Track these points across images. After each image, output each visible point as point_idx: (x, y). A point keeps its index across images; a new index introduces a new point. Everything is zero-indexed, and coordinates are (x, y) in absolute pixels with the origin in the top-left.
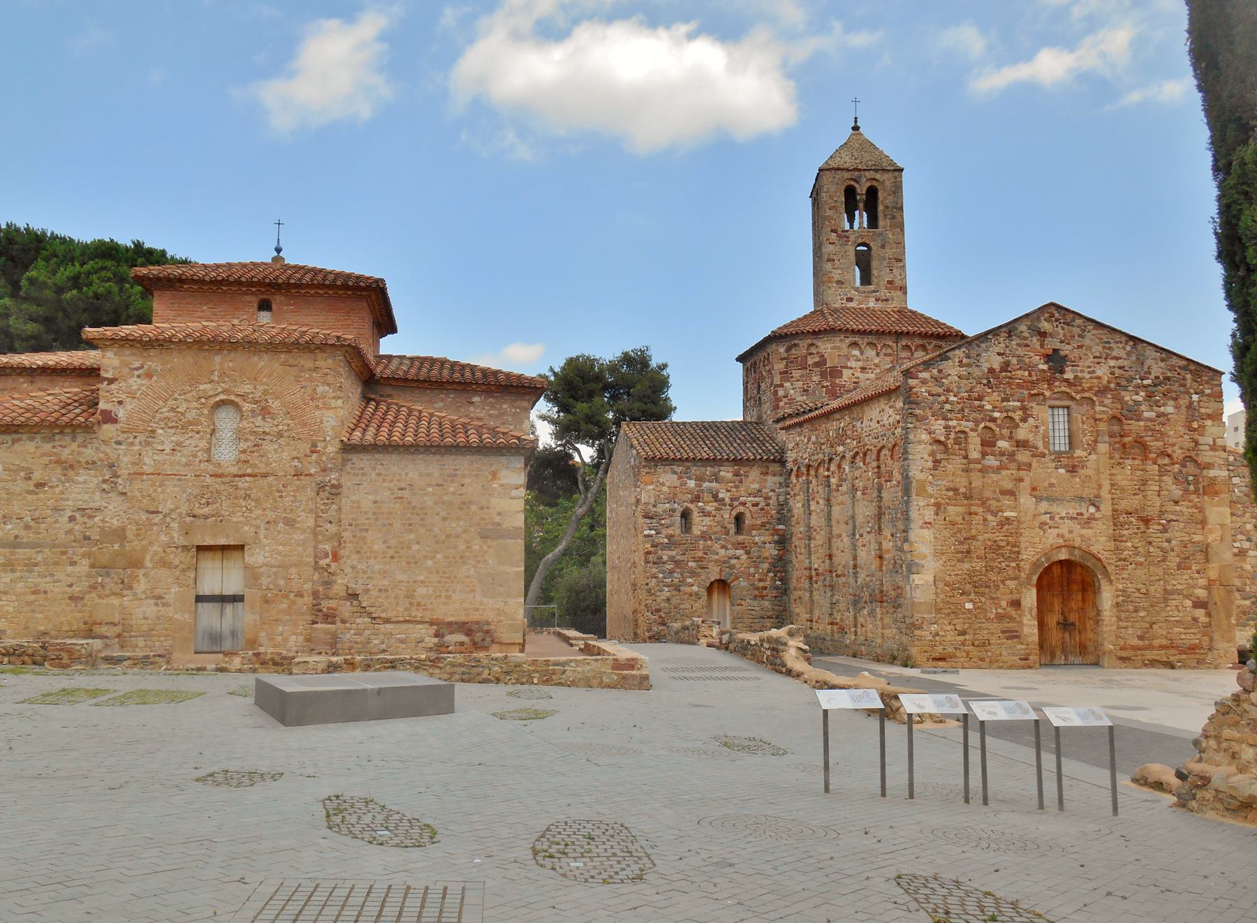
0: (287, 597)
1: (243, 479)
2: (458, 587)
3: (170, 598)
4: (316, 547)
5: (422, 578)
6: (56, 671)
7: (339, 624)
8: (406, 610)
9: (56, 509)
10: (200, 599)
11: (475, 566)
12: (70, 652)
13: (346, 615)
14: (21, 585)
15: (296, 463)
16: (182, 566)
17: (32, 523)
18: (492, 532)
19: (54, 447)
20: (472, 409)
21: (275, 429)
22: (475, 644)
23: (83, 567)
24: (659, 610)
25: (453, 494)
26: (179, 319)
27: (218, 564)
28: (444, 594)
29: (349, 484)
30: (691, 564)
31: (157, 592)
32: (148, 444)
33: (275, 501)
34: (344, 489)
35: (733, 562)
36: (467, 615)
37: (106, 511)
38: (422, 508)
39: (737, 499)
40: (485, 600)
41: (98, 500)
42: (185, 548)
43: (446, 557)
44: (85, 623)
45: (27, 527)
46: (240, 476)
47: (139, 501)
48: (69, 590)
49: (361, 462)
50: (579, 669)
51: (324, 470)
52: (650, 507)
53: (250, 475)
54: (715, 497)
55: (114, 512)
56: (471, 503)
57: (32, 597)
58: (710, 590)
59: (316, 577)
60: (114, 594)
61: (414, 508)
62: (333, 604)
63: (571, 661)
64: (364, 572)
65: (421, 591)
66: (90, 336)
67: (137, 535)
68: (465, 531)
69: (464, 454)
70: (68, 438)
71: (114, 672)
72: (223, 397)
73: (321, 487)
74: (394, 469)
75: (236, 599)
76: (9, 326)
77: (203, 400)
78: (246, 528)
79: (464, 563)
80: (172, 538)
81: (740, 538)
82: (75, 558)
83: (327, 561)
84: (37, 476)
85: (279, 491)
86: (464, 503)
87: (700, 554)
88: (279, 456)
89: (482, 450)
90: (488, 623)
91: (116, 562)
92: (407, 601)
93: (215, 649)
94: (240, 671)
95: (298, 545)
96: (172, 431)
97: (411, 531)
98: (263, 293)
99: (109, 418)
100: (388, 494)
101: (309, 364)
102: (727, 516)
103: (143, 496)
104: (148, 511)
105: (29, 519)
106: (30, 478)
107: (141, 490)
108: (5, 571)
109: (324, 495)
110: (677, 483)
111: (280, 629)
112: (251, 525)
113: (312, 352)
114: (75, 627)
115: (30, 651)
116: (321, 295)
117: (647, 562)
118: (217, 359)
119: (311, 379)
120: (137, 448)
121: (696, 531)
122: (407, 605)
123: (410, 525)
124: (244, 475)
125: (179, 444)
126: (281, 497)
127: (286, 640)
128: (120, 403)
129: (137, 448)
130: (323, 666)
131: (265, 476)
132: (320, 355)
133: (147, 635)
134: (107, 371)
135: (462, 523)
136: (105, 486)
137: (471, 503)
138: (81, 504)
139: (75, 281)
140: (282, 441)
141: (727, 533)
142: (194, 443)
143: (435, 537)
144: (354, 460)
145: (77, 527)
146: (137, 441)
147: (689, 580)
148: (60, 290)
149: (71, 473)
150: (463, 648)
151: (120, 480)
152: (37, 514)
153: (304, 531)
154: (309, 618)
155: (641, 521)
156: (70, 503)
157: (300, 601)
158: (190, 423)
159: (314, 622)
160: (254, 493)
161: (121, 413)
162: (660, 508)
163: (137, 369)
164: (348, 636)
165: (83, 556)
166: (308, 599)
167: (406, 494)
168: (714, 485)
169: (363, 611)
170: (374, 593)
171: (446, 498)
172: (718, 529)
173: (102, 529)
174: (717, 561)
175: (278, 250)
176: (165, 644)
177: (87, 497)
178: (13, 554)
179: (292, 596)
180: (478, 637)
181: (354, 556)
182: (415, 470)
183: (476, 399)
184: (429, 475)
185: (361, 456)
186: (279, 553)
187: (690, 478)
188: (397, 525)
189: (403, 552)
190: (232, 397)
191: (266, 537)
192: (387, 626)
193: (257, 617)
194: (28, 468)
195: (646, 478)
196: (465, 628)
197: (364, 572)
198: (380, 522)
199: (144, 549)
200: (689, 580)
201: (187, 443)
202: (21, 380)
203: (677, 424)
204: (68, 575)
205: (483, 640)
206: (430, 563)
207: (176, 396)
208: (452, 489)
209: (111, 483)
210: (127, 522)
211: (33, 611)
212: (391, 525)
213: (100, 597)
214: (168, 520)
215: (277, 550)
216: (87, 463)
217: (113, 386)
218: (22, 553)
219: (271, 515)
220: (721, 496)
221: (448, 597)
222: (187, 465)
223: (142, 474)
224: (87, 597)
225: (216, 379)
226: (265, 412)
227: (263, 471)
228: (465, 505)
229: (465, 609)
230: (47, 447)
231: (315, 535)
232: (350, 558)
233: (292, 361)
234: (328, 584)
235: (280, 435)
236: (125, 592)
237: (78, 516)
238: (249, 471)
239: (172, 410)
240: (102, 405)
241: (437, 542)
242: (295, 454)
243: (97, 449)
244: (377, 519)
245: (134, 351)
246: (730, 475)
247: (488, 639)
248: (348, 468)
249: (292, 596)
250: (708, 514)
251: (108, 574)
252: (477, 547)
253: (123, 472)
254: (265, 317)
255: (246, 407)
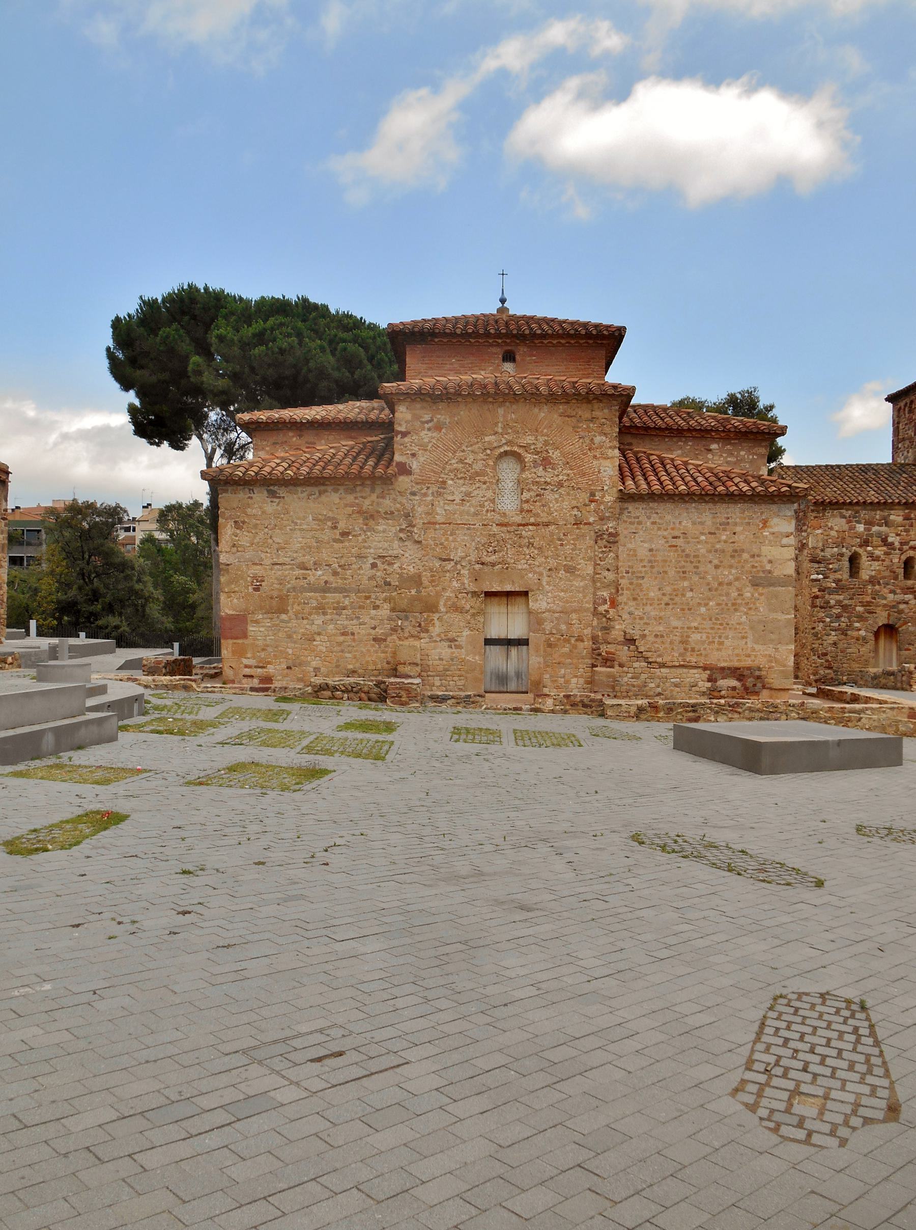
0: (568, 641)
1: (527, 528)
2: (731, 634)
3: (462, 640)
4: (595, 594)
5: (696, 624)
6: (397, 707)
7: (617, 667)
8: (681, 655)
9: (360, 557)
10: (489, 642)
11: (746, 614)
12: (408, 691)
13: (624, 659)
14: (331, 626)
15: (575, 512)
16: (472, 611)
17: (339, 570)
18: (763, 580)
19: (356, 498)
20: (710, 456)
21: (556, 479)
22: (746, 689)
23: (385, 611)
24: (825, 654)
25: (725, 542)
26: (430, 372)
27: (503, 609)
28: (716, 640)
29: (626, 532)
30: (858, 609)
31: (450, 635)
32: (440, 494)
33: (556, 549)
34: (621, 538)
35: (902, 606)
36: (739, 660)
37: (404, 559)
38: (695, 556)
39: (906, 543)
40: (756, 646)
41: (396, 548)
42: (475, 594)
43: (718, 604)
44: (388, 663)
45: (335, 573)
46: (524, 525)
47: (434, 549)
48: (373, 632)
49: (636, 510)
50: (875, 717)
51: (602, 519)
52: (818, 551)
53: (532, 524)
54: (885, 541)
55: (410, 560)
56: (743, 551)
57: (342, 638)
58: (877, 634)
59: (595, 623)
60: (412, 636)
61: (687, 556)
62: (611, 648)
63: (867, 709)
64: (641, 618)
65: (695, 637)
66: (388, 391)
67: (433, 581)
68: (737, 579)
69: (736, 502)
70: (368, 490)
71: (440, 709)
72: (506, 448)
73: (599, 536)
74: (668, 517)
75: (522, 642)
76: (202, 383)
77: (488, 452)
78: (530, 575)
79: (736, 610)
80: (463, 584)
81: (910, 583)
82: (378, 603)
83: (606, 607)
84: (342, 525)
85: (560, 540)
86: (735, 551)
87: (868, 599)
88: (560, 506)
89: (754, 498)
90: (759, 669)
91: (414, 607)
92: (682, 646)
93: (502, 689)
94: (553, 711)
95: (579, 592)
96: (461, 481)
97: (684, 579)
98: (507, 344)
99: (404, 470)
100: (662, 542)
101: (587, 415)
102: (897, 559)
103: (436, 545)
104: (440, 559)
105: (336, 565)
106: (336, 528)
107: (434, 539)
108: (318, 614)
109: (602, 543)
110: (846, 527)
111: (563, 671)
112: (535, 572)
113: (589, 402)
114: (379, 666)
115: (366, 689)
116: (563, 345)
117: (814, 606)
118: (501, 411)
119: (588, 430)
120: (430, 498)
121: (865, 575)
122: (682, 650)
123: (684, 572)
124: (527, 524)
125: (468, 494)
126: (562, 545)
127: (567, 682)
128: (414, 455)
129: (430, 498)
130: (633, 710)
131: (547, 525)
132: (596, 405)
133: (442, 675)
134: (400, 425)
135: (734, 571)
136: (401, 535)
137: (743, 551)
138: (381, 552)
139: (260, 338)
140: (562, 490)
141: (896, 578)
142: (481, 493)
143: (708, 584)
144: (630, 509)
145: (379, 574)
146: (430, 491)
147: (857, 625)
148: (245, 346)
149: (371, 523)
150: (735, 693)
151: (415, 530)
152: (343, 562)
153: (584, 579)
154: (589, 661)
155: (806, 565)
156: (372, 551)
157: (581, 645)
158: (477, 474)
159: (594, 666)
160: (537, 542)
161: (415, 465)
162: (828, 553)
163: (427, 422)
164: (626, 679)
165: (385, 600)
166: (588, 644)
167: (680, 542)
168: (884, 529)
169: (640, 655)
170: (651, 638)
171: (718, 546)
172: (887, 573)
173: (401, 575)
174: (885, 606)
175: (503, 301)
176: (459, 683)
177: (386, 545)
178: (324, 598)
179: (573, 640)
180: (750, 682)
181: (632, 603)
182: (691, 520)
183: (714, 446)
184: (702, 523)
185: (637, 505)
186: (561, 599)
187: (859, 522)
188: (672, 573)
189: (677, 599)
190: (516, 449)
191: (548, 583)
192: (663, 670)
193: (542, 660)
194: (333, 518)
195: (815, 522)
196: (736, 673)
197: (641, 618)
198: (655, 570)
199: (438, 595)
200: (857, 625)
201: (476, 492)
202: (291, 434)
203: (788, 467)
204: (372, 618)
205: (755, 685)
206: (703, 610)
207: (464, 447)
208: (724, 537)
209: (407, 534)
210: (422, 569)
211: (342, 651)
212: (665, 572)
213: (400, 639)
214: (459, 567)
215: (560, 596)
216: (386, 513)
217: (406, 439)
218: (331, 597)
219: (552, 563)
220: (890, 540)
221: (721, 643)
222: (476, 514)
223: (435, 523)
224: (389, 639)
225: (500, 430)
226: (546, 462)
227: (546, 520)
228: (737, 553)
229: (737, 655)
230: (350, 498)
231: (594, 581)
232: (627, 605)
233: (570, 412)
234: (606, 629)
235: (560, 485)
236: (422, 635)
237: (378, 562)
238: (532, 520)
239: (461, 461)
240: (397, 458)
241: (710, 590)
242: (574, 503)
243: (395, 500)
244: (652, 567)
245: (425, 404)
246: (900, 519)
247: (759, 685)
248: (624, 517)
249: (573, 640)
250: (877, 559)
251: (407, 618)
252: (749, 595)
253: (419, 522)
254: (509, 367)
255: (529, 457)
